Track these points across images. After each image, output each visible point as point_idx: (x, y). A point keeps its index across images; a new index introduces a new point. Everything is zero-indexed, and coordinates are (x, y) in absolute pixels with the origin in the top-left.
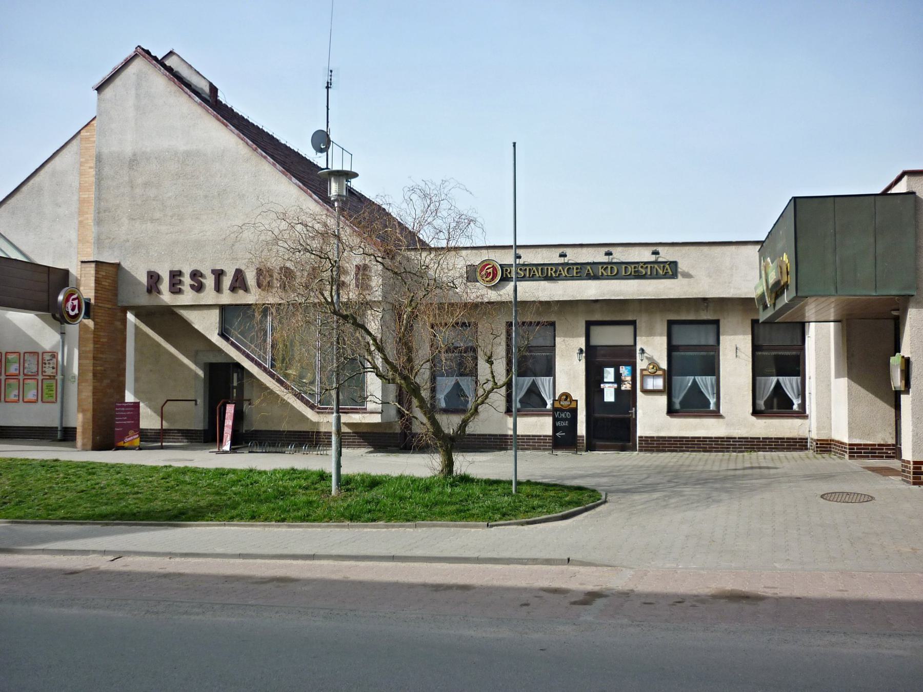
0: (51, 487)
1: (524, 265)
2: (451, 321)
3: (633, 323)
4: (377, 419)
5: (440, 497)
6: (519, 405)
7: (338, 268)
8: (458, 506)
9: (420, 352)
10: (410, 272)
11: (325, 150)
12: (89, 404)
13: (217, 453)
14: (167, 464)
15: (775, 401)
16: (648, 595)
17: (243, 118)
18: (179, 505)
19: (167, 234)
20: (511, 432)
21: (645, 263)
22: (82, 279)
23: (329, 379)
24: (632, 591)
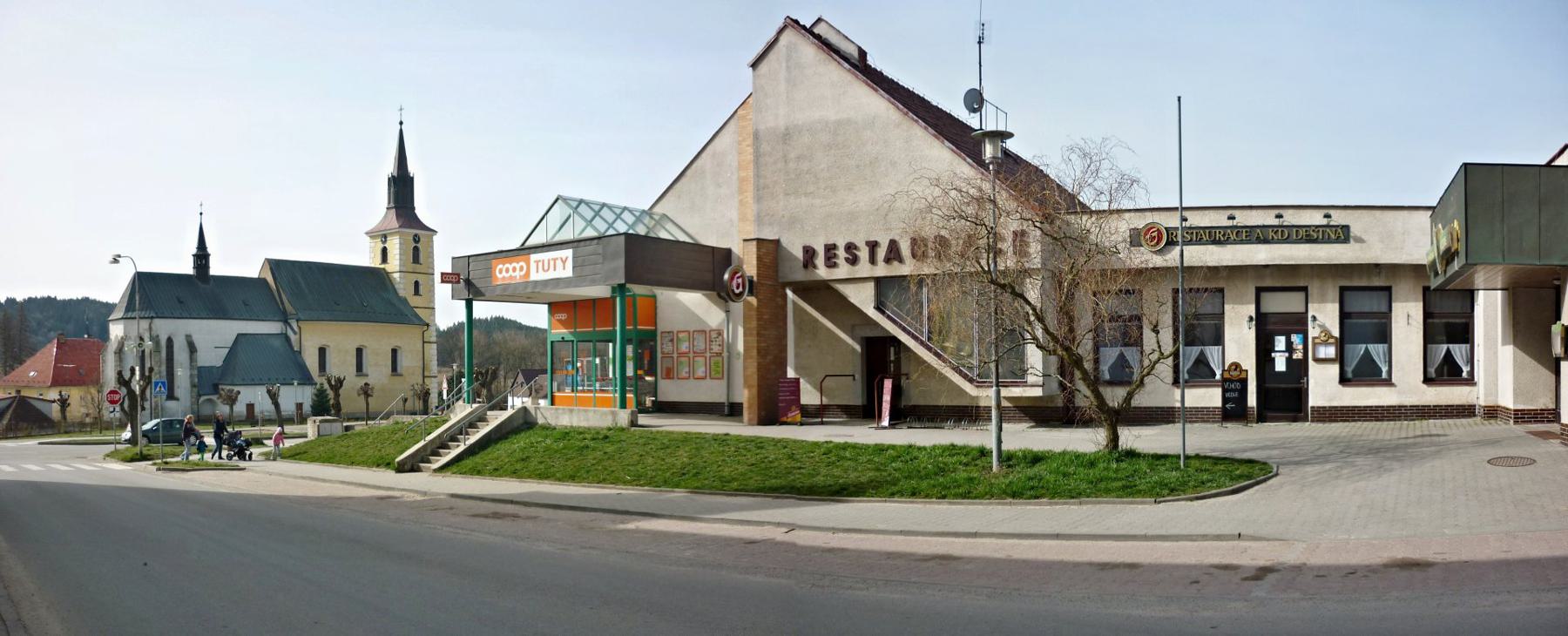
0: (723, 460)
1: (1190, 228)
2: (1115, 288)
3: (1305, 289)
4: (1038, 392)
5: (1106, 473)
6: (1186, 376)
7: (994, 235)
8: (1124, 482)
9: (1082, 321)
10: (1070, 238)
11: (979, 110)
12: (754, 381)
13: (876, 428)
14: (828, 439)
15: (1445, 368)
16: (1320, 568)
17: (893, 81)
18: (841, 481)
19: (821, 207)
20: (1178, 405)
21: (1317, 227)
22: (746, 257)
23: (988, 351)
24: (1305, 564)
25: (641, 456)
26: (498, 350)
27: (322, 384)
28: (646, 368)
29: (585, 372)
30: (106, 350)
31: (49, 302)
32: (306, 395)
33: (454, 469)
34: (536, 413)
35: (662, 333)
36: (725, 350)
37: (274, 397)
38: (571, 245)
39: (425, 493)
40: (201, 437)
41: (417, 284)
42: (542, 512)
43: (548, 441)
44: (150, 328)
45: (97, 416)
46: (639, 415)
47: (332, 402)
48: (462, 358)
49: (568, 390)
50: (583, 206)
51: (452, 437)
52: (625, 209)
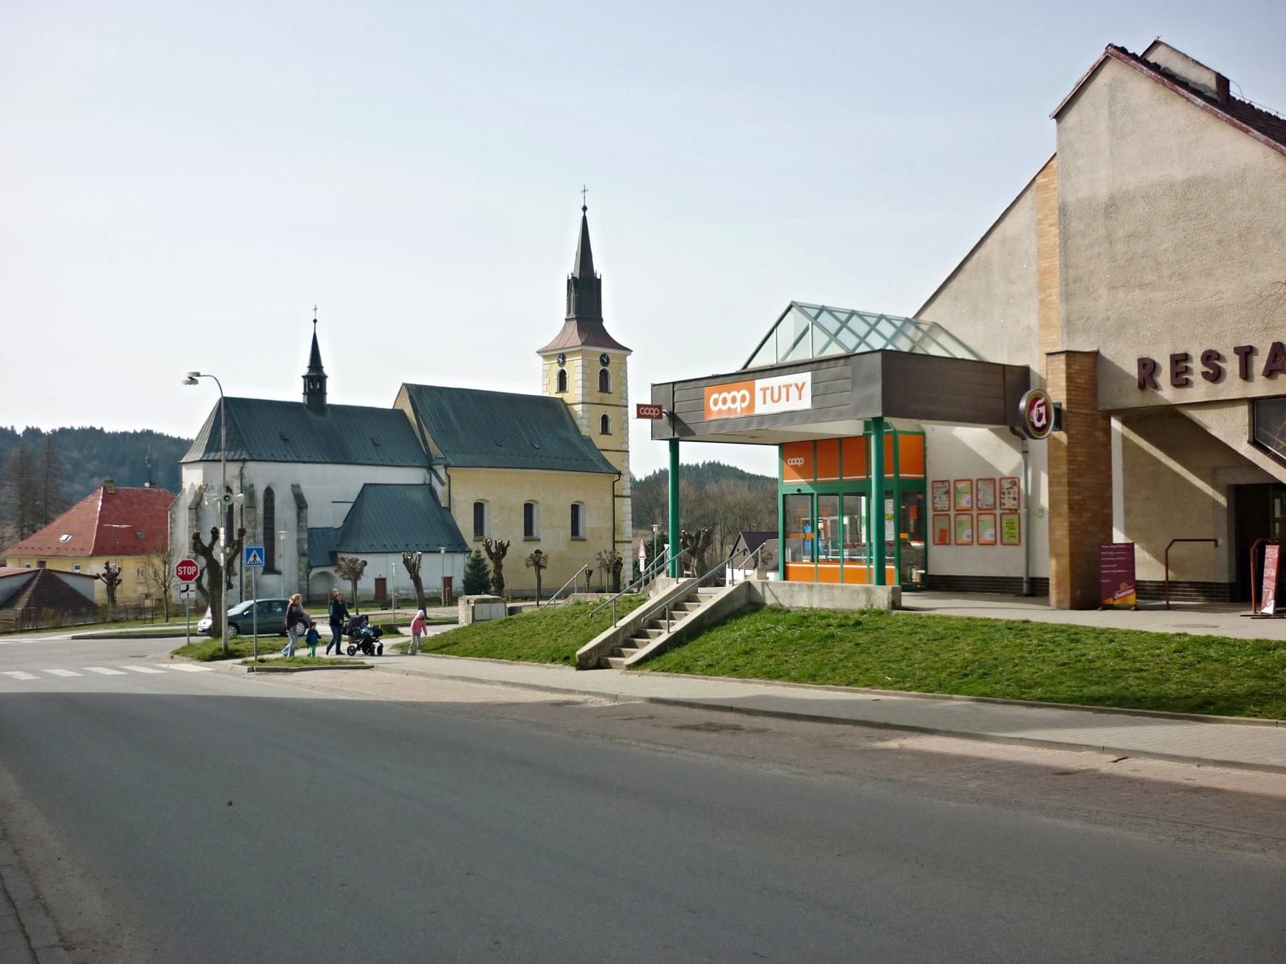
0: (1022, 657)
12: (1065, 546)
13: (1254, 617)
14: (1181, 631)
22: (1050, 377)
25: (906, 649)
26: (712, 506)
27: (478, 552)
28: (912, 531)
29: (829, 535)
30: (176, 504)
31: (93, 435)
32: (457, 567)
33: (655, 664)
34: (763, 592)
35: (933, 482)
36: (1023, 505)
37: (413, 569)
38: (808, 367)
39: (616, 698)
40: (310, 624)
41: (605, 419)
42: (771, 723)
43: (780, 628)
44: (242, 475)
45: (162, 597)
46: (903, 593)
47: (491, 575)
48: (665, 517)
49: (806, 559)
50: (825, 315)
51: (654, 621)
52: (882, 317)
